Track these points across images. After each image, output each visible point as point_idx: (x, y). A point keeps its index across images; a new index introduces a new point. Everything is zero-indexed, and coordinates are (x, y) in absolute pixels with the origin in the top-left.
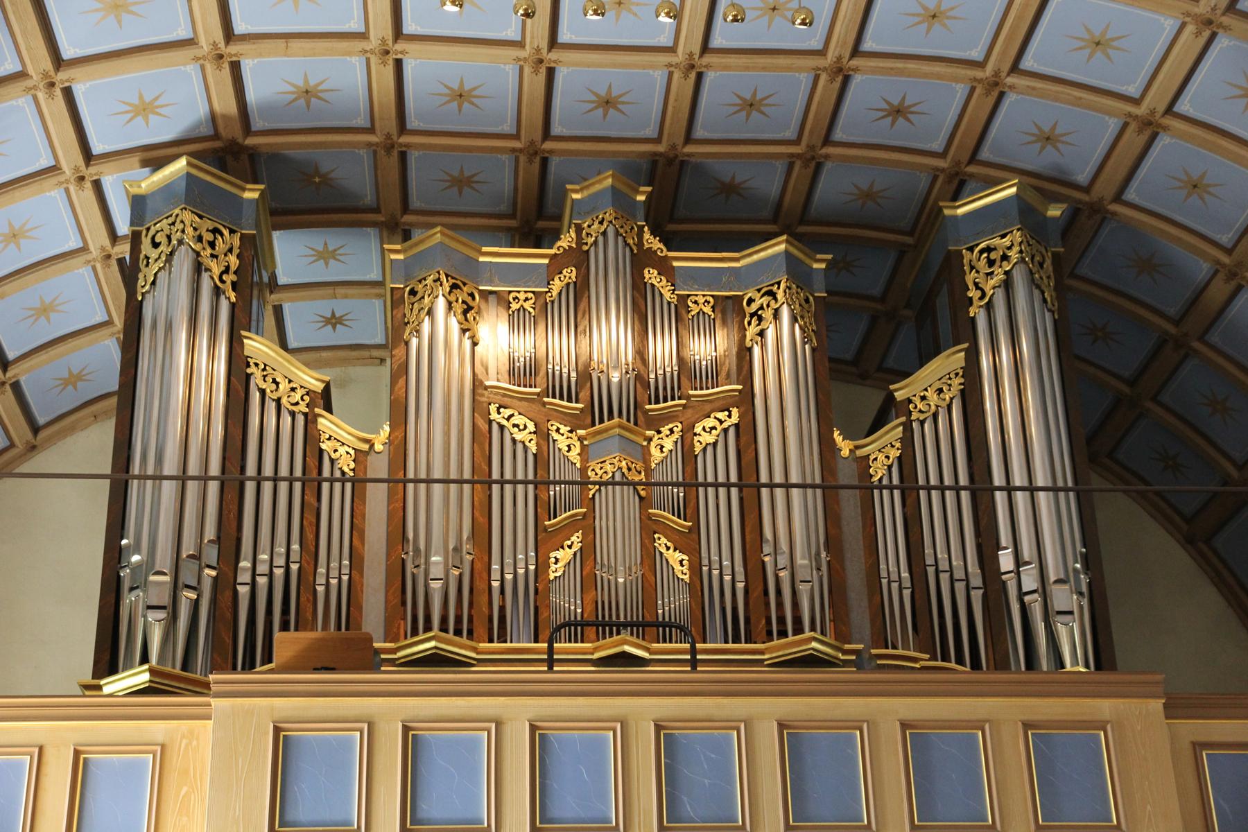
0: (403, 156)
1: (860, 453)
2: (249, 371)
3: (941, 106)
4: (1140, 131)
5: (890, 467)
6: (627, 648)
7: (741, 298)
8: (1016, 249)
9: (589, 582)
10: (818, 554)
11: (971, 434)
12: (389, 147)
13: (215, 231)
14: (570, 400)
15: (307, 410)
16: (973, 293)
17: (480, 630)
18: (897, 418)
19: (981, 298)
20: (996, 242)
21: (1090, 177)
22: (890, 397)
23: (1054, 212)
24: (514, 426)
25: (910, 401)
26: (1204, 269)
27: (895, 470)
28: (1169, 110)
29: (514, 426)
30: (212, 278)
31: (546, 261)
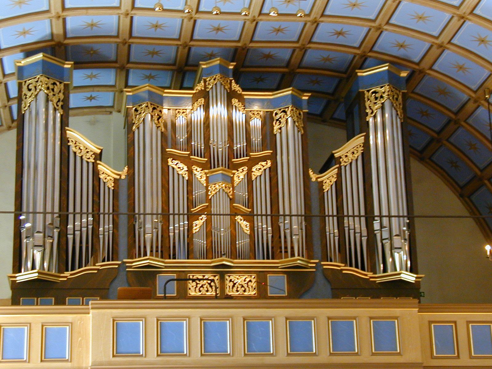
0: (129, 46)
1: (319, 180)
2: (69, 144)
3: (356, 34)
4: (438, 48)
5: (332, 185)
6: (224, 263)
7: (272, 112)
8: (386, 94)
9: (209, 234)
10: (301, 223)
11: (366, 172)
12: (124, 43)
13: (54, 84)
14: (201, 157)
15: (93, 161)
16: (368, 111)
17: (166, 254)
18: (336, 165)
19: (372, 113)
20: (378, 89)
21: (419, 60)
22: (332, 155)
23: (404, 74)
24: (179, 168)
25: (340, 157)
26: (465, 98)
27: (334, 187)
28: (449, 42)
29: (179, 168)
30: (53, 104)
31: (191, 96)
